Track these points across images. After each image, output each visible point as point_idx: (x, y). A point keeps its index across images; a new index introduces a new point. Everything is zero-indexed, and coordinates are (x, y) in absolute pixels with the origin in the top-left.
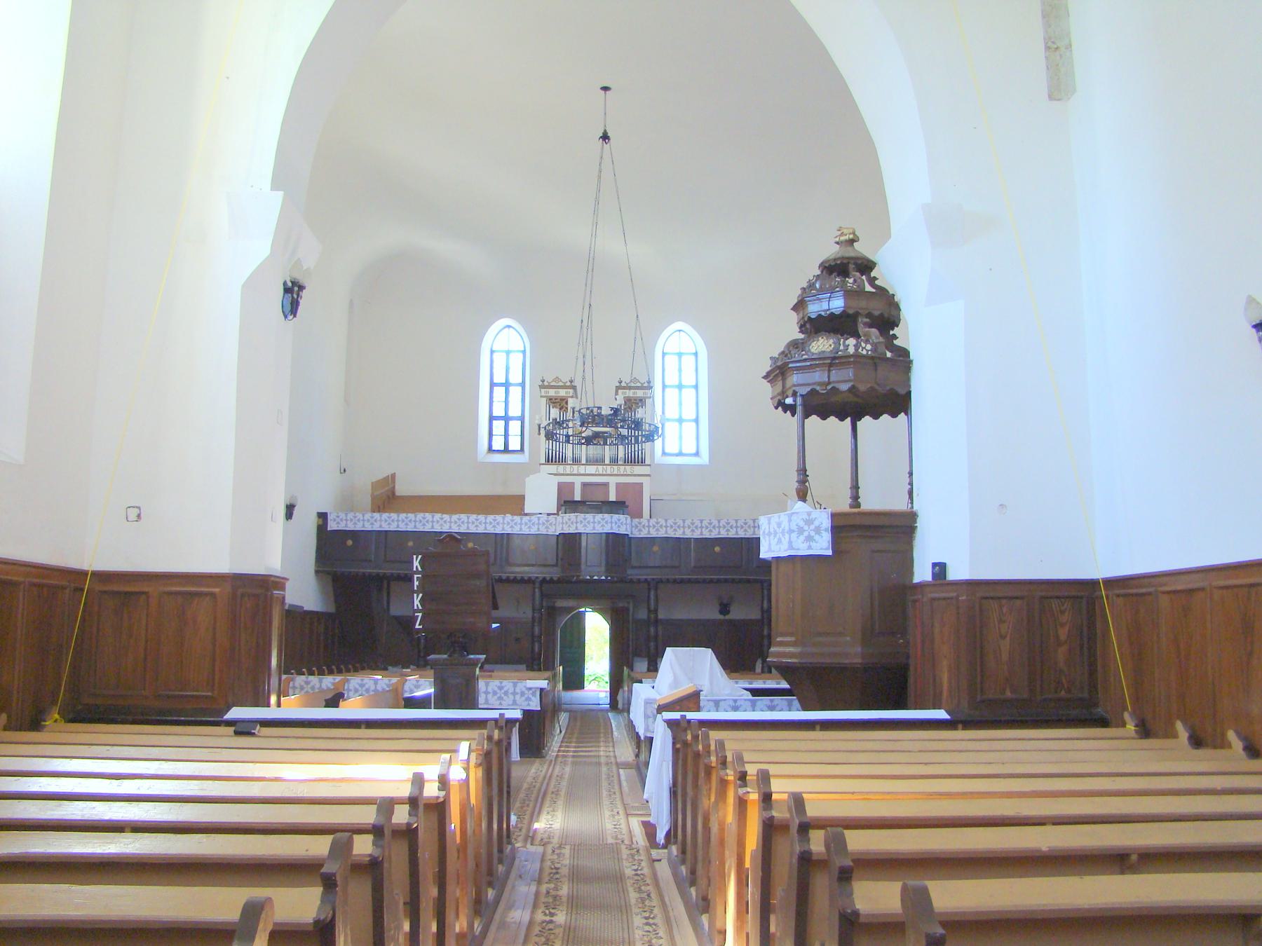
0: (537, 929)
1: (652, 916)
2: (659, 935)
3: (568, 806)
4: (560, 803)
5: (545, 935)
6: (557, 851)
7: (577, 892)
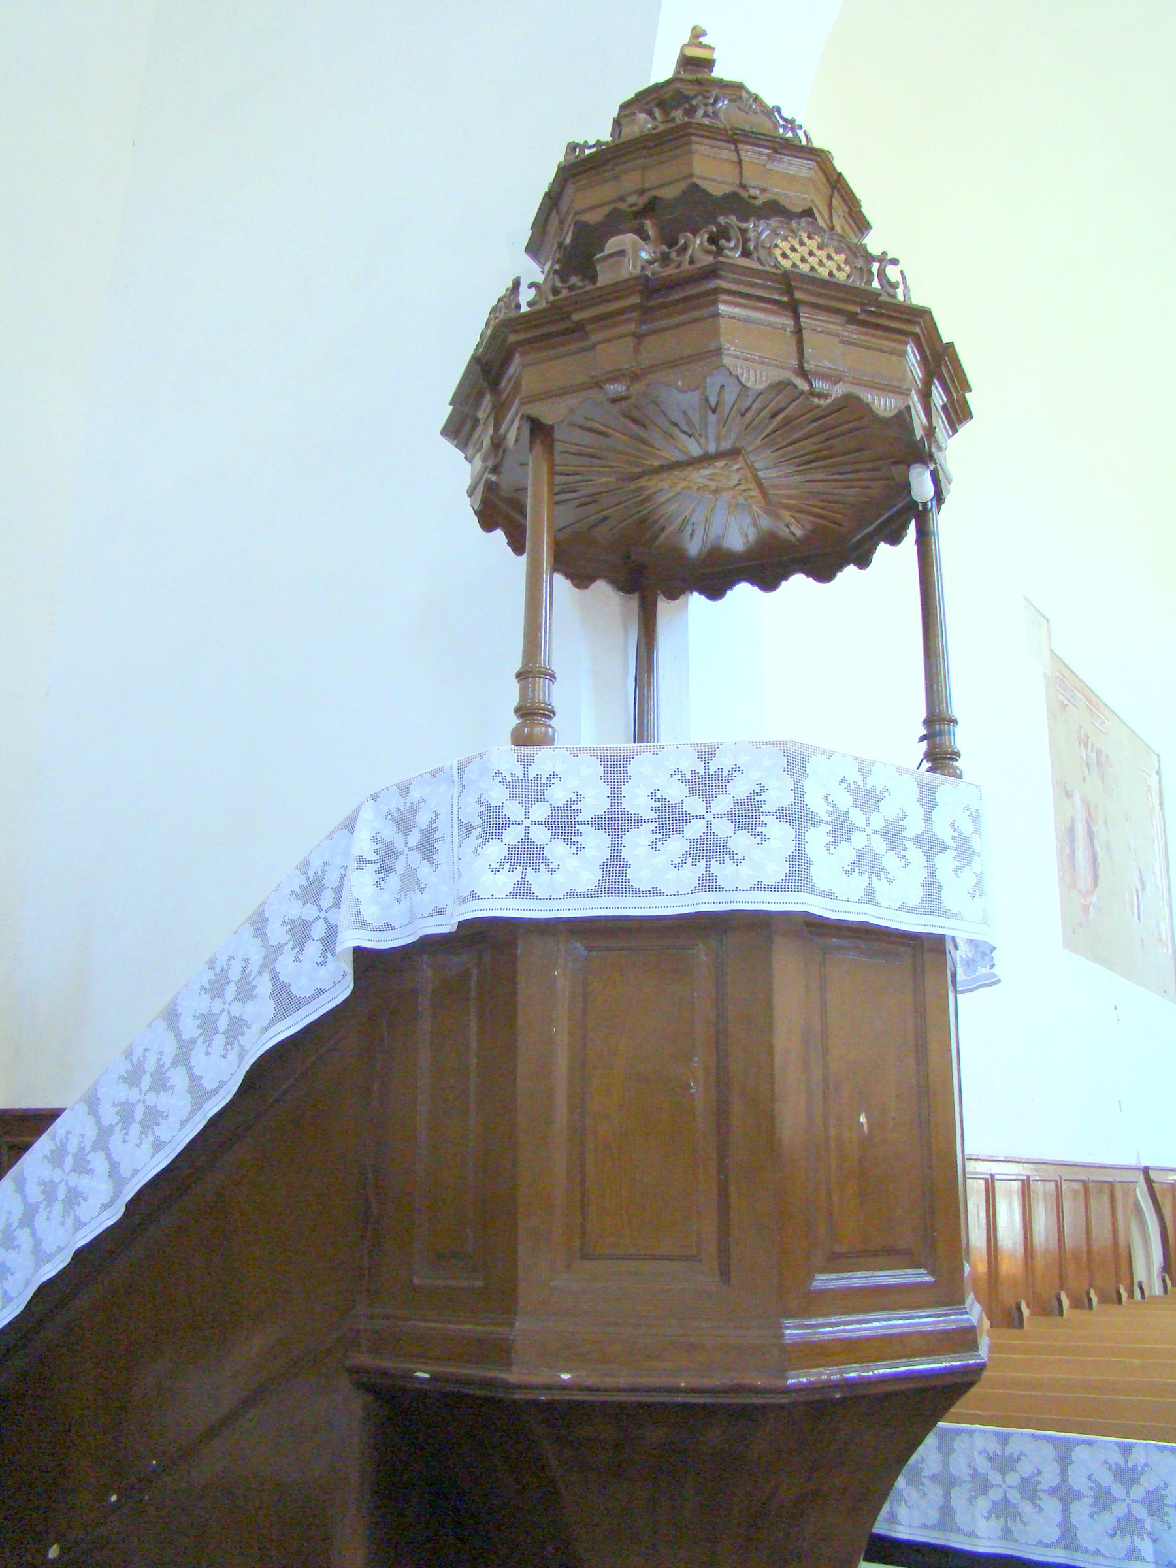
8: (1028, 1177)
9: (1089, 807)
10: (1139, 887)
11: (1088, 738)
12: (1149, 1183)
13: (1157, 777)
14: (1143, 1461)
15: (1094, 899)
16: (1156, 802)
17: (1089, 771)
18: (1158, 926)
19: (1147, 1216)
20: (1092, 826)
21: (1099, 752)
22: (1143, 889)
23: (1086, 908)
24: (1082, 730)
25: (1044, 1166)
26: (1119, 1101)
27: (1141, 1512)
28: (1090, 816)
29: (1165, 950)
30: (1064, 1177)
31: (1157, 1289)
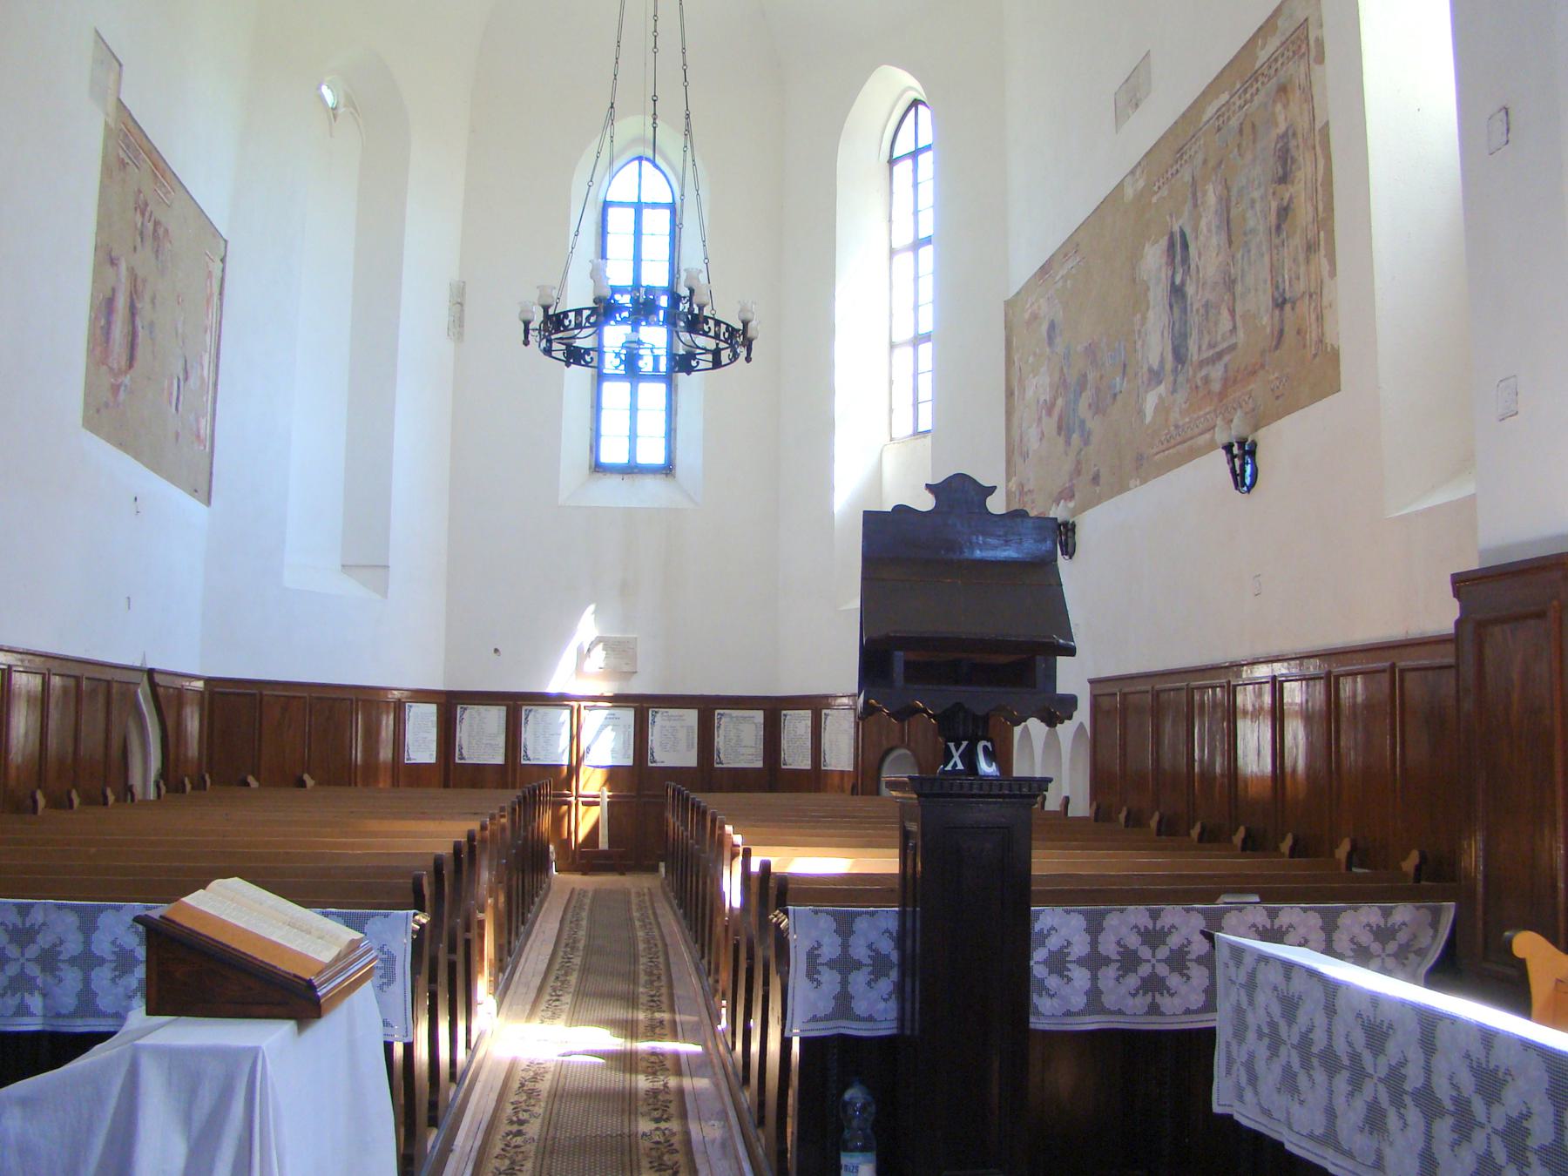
0: (673, 1109)
1: (665, 1116)
2: (673, 1147)
3: (579, 1001)
4: (567, 998)
5: (660, 1103)
6: (655, 978)
7: (622, 1121)
8: (10, 667)
9: (135, 280)
10: (181, 377)
11: (146, 205)
12: (153, 685)
13: (221, 265)
14: (40, 920)
15: (127, 380)
16: (216, 290)
17: (142, 241)
18: (197, 421)
19: (148, 720)
20: (136, 301)
21: (157, 224)
22: (186, 379)
23: (116, 389)
24: (142, 195)
25: (30, 657)
26: (129, 598)
27: (34, 970)
28: (136, 292)
29: (202, 448)
30: (53, 671)
31: (152, 795)
